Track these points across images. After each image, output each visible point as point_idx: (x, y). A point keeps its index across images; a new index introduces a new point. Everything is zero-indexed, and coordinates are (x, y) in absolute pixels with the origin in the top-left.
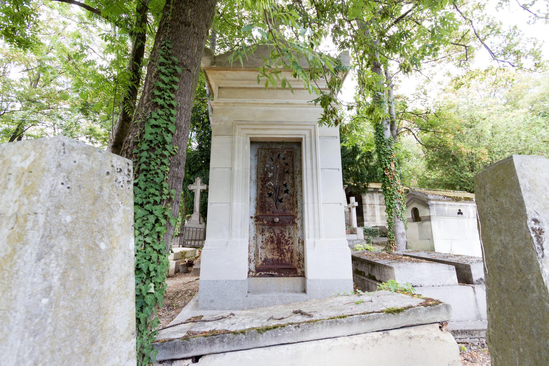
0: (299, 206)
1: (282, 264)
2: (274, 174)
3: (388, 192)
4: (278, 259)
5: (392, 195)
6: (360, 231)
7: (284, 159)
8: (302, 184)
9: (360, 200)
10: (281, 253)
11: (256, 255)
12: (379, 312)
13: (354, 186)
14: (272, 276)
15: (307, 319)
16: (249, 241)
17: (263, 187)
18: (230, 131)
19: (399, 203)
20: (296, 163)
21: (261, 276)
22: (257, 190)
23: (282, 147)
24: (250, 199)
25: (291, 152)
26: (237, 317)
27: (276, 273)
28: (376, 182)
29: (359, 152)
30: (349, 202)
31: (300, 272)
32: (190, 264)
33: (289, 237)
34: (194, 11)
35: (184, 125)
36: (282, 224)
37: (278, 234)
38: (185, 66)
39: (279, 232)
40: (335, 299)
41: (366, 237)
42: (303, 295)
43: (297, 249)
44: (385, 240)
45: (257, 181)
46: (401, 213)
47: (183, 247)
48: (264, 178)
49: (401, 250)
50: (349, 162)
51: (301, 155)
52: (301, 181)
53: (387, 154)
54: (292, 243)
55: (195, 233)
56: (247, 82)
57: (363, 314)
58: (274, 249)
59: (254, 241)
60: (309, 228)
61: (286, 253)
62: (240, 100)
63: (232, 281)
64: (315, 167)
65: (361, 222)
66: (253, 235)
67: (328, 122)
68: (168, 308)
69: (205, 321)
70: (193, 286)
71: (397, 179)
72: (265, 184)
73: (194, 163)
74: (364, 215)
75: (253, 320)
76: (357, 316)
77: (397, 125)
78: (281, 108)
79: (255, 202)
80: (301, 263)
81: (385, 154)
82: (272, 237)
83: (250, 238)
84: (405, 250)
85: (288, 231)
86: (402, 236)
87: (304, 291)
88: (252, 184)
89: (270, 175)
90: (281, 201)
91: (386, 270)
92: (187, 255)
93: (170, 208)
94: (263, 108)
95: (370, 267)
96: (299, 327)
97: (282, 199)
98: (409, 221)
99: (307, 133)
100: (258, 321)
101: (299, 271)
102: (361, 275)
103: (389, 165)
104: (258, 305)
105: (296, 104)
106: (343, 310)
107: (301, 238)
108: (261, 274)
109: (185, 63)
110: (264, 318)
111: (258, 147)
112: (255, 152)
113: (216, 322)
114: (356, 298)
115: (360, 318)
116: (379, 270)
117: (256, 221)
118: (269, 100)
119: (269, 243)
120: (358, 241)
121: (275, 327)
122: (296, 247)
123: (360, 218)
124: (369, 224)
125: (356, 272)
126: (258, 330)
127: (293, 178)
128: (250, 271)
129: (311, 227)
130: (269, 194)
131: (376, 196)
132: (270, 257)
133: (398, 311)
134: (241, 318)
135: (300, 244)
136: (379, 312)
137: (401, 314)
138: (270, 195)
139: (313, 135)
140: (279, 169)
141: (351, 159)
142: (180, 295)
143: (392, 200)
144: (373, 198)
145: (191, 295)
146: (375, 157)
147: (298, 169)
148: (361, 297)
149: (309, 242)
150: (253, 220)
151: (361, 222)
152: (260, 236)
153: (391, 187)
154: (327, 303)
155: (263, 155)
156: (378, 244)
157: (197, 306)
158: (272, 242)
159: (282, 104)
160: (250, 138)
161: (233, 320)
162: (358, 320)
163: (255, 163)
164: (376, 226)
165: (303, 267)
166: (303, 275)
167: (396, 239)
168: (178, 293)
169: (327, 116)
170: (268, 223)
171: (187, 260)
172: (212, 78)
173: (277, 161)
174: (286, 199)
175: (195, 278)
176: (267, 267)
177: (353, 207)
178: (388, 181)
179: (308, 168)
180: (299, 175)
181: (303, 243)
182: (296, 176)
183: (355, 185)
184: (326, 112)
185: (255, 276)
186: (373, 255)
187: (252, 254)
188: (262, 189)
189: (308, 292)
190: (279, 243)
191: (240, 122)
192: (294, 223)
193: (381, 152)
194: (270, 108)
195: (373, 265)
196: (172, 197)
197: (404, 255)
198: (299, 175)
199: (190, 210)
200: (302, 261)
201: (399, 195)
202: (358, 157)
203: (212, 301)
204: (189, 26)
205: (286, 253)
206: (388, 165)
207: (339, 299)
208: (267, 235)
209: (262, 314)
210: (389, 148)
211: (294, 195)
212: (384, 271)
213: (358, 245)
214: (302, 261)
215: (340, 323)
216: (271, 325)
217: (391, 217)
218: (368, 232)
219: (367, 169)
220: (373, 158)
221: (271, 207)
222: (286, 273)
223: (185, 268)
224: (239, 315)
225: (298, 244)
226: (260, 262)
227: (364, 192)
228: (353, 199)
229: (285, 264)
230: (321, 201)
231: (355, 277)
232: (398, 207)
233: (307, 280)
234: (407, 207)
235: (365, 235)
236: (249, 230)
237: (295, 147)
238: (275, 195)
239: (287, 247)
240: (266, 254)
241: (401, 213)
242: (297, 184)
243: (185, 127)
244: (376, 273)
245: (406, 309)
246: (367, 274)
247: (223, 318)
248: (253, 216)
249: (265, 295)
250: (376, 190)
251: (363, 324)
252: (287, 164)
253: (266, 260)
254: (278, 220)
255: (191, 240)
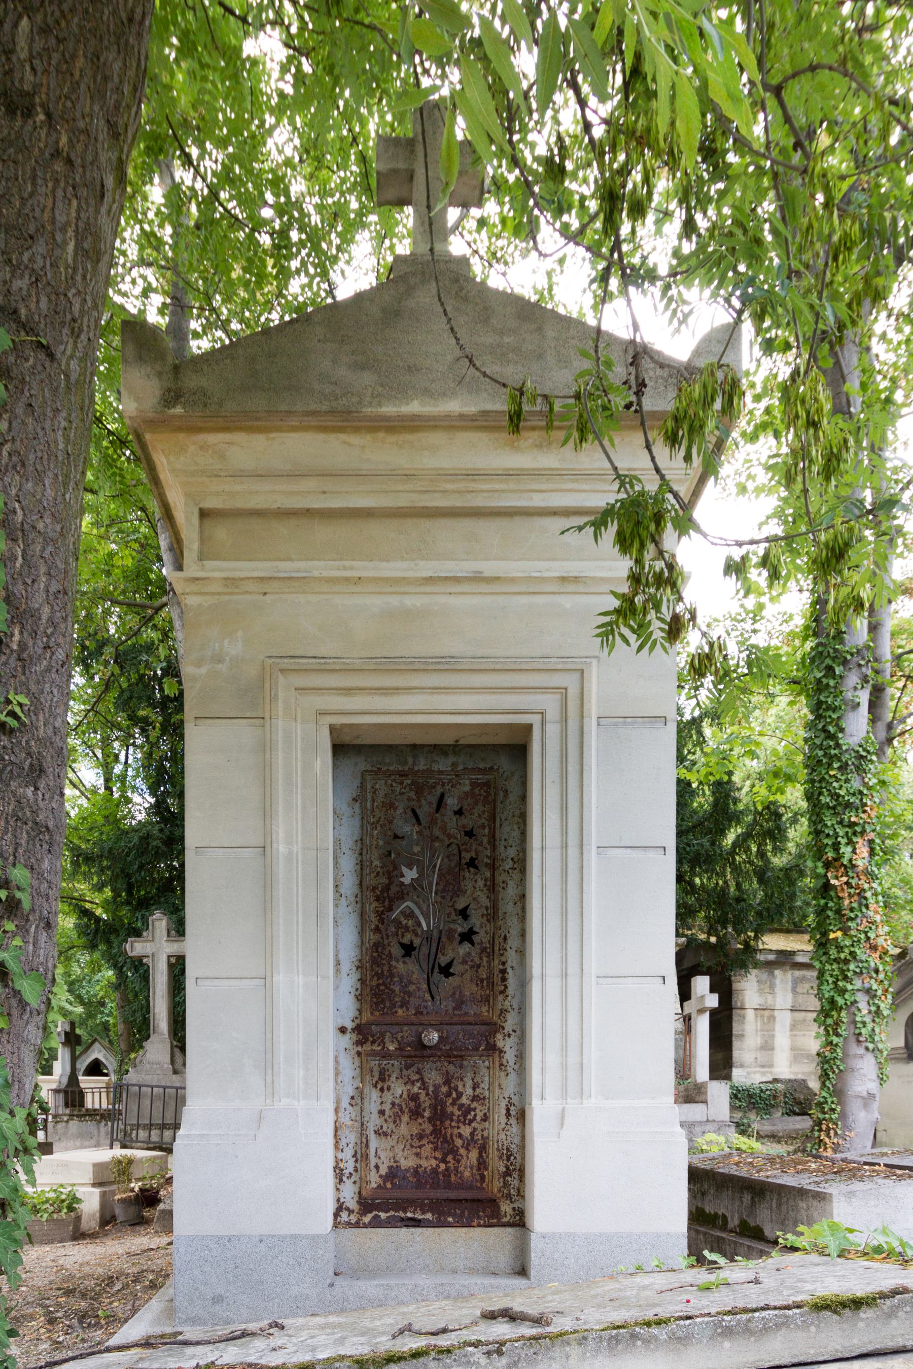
0: (511, 990)
1: (448, 1186)
2: (421, 873)
3: (833, 952)
4: (435, 1171)
5: (846, 961)
6: (719, 1093)
7: (459, 813)
8: (524, 909)
9: (723, 988)
10: (446, 1148)
11: (361, 1156)
12: (788, 1308)
13: (707, 942)
14: (416, 1223)
15: (528, 1330)
16: (336, 1111)
17: (382, 921)
18: (252, 701)
19: (868, 991)
20: (506, 828)
21: (376, 1223)
22: (362, 933)
23: (454, 765)
24: (338, 963)
25: (487, 784)
26: (291, 1332)
27: (429, 1216)
28: (788, 931)
29: (736, 818)
30: (685, 994)
31: (509, 1211)
32: (149, 1199)
33: (475, 1098)
34: (45, 30)
35: (46, 611)
36: (451, 1053)
37: (437, 1087)
38: (27, 327)
39: (439, 1080)
40: (628, 1281)
41: (738, 1115)
42: (520, 1282)
43: (502, 1136)
44: (803, 1123)
45: (360, 900)
46: (870, 1026)
47: (124, 1146)
48: (387, 888)
49: (858, 1145)
50: (698, 854)
51: (524, 798)
52: (522, 898)
53: (848, 805)
54: (485, 1118)
55: (158, 1105)
56: (311, 484)
57: (729, 1313)
58: (421, 1137)
59: (353, 1112)
60: (543, 1063)
61: (462, 1151)
62: (286, 568)
63: (282, 1238)
64: (575, 840)
65: (722, 1065)
66: (350, 1090)
67: (641, 629)
68: (81, 1322)
69: (186, 1343)
70: (159, 1262)
71: (871, 901)
72: (390, 909)
73: (141, 867)
74: (736, 1044)
75: (344, 1338)
76: (706, 1319)
77: (892, 704)
78: (452, 601)
79: (355, 976)
80: (514, 1181)
81: (841, 805)
82: (414, 1098)
83: (338, 1101)
84: (869, 1150)
85: (470, 1075)
86: (866, 1105)
87: (522, 1271)
88: (343, 909)
89: (410, 875)
90: (446, 971)
91: (803, 1205)
92: (136, 1172)
93: (17, 942)
94: (376, 602)
95: (747, 1198)
96: (500, 1353)
97: (450, 965)
98: (893, 1057)
99: (550, 704)
100: (363, 1339)
101: (506, 1207)
102: (714, 1226)
103: (849, 849)
104: (364, 1305)
105: (513, 580)
106: (655, 1305)
107: (515, 1099)
108: (377, 1216)
109: (23, 312)
110: (383, 1333)
111: (363, 766)
112: (351, 790)
113: (222, 1346)
114: (702, 1276)
115: (718, 1325)
116: (779, 1205)
117: (359, 1043)
118: (405, 564)
119: (405, 1118)
120: (709, 1127)
121: (416, 1355)
122: (498, 1129)
123: (720, 1056)
124: (746, 1074)
125: (699, 1218)
126: (357, 1362)
127: (492, 888)
128: (340, 1208)
129: (553, 1060)
130: (403, 946)
131: (783, 978)
132: (407, 1162)
133: (857, 1304)
134: (304, 1335)
135: (513, 1121)
136: (788, 1308)
137: (866, 1314)
138: (408, 949)
139: (573, 709)
140: (441, 833)
141: (705, 842)
142: (118, 1286)
143: (846, 978)
144: (772, 987)
145: (154, 1286)
146: (798, 834)
147: (512, 852)
148: (723, 1274)
149: (541, 1113)
150: (347, 1040)
151: (722, 1065)
152: (375, 1095)
153: (845, 931)
154: (599, 1291)
155: (380, 799)
156: (774, 1137)
157: (170, 1312)
158: (416, 1114)
159: (457, 580)
160: (332, 729)
161: (278, 1339)
162: (708, 1332)
163: (350, 831)
164: (776, 1081)
165: (521, 1194)
166: (520, 1221)
167: (843, 1116)
168: (111, 1281)
169: (639, 600)
170: (400, 1049)
171: (136, 1186)
172: (173, 471)
173: (433, 821)
174: (464, 962)
175: (165, 1240)
176: (397, 1194)
177: (701, 1011)
178: (838, 912)
179: (548, 843)
180: (516, 875)
181: (522, 1117)
182: (504, 877)
183: (713, 939)
184: (635, 579)
185: (357, 1225)
186: (759, 1162)
187: (348, 1154)
188: (377, 930)
189: (533, 1273)
190: (439, 1115)
191: (292, 663)
192: (493, 1049)
193: (825, 799)
194: (410, 601)
195: (759, 1190)
196: (18, 895)
197: (866, 1163)
198: (516, 875)
199: (138, 1030)
200: (516, 1175)
201: (874, 960)
202: (731, 837)
203: (218, 1299)
204: (28, 113)
205: (462, 1151)
206: (846, 850)
207: (641, 1280)
208: (399, 1089)
209: (378, 1323)
210: (856, 784)
211: (493, 949)
212: (796, 1209)
213: (711, 1136)
214: (516, 1175)
215: (646, 1342)
216: (405, 1349)
217: (835, 1040)
218: (748, 1101)
219: (761, 881)
220: (785, 839)
221: (410, 994)
222: (462, 1216)
223: (132, 1210)
224: (300, 1328)
225: (503, 1120)
226: (374, 1180)
227: (743, 966)
228: (701, 984)
229: (460, 1186)
230: (593, 967)
231: (693, 1233)
232: (863, 1005)
233: (533, 1236)
234: (895, 1006)
235: (733, 1108)
236: (337, 1074)
237: (504, 763)
238: (425, 950)
239: (466, 1131)
240: (393, 1152)
241: (870, 1026)
242: (508, 907)
243: (50, 620)
244: (764, 1218)
245: (883, 1296)
246: (734, 1222)
247: (244, 1334)
248: (349, 1025)
249: (392, 1282)
250: (785, 959)
251: (727, 1344)
252: (470, 834)
253: (393, 1173)
254: (435, 1036)
255: (150, 1127)
